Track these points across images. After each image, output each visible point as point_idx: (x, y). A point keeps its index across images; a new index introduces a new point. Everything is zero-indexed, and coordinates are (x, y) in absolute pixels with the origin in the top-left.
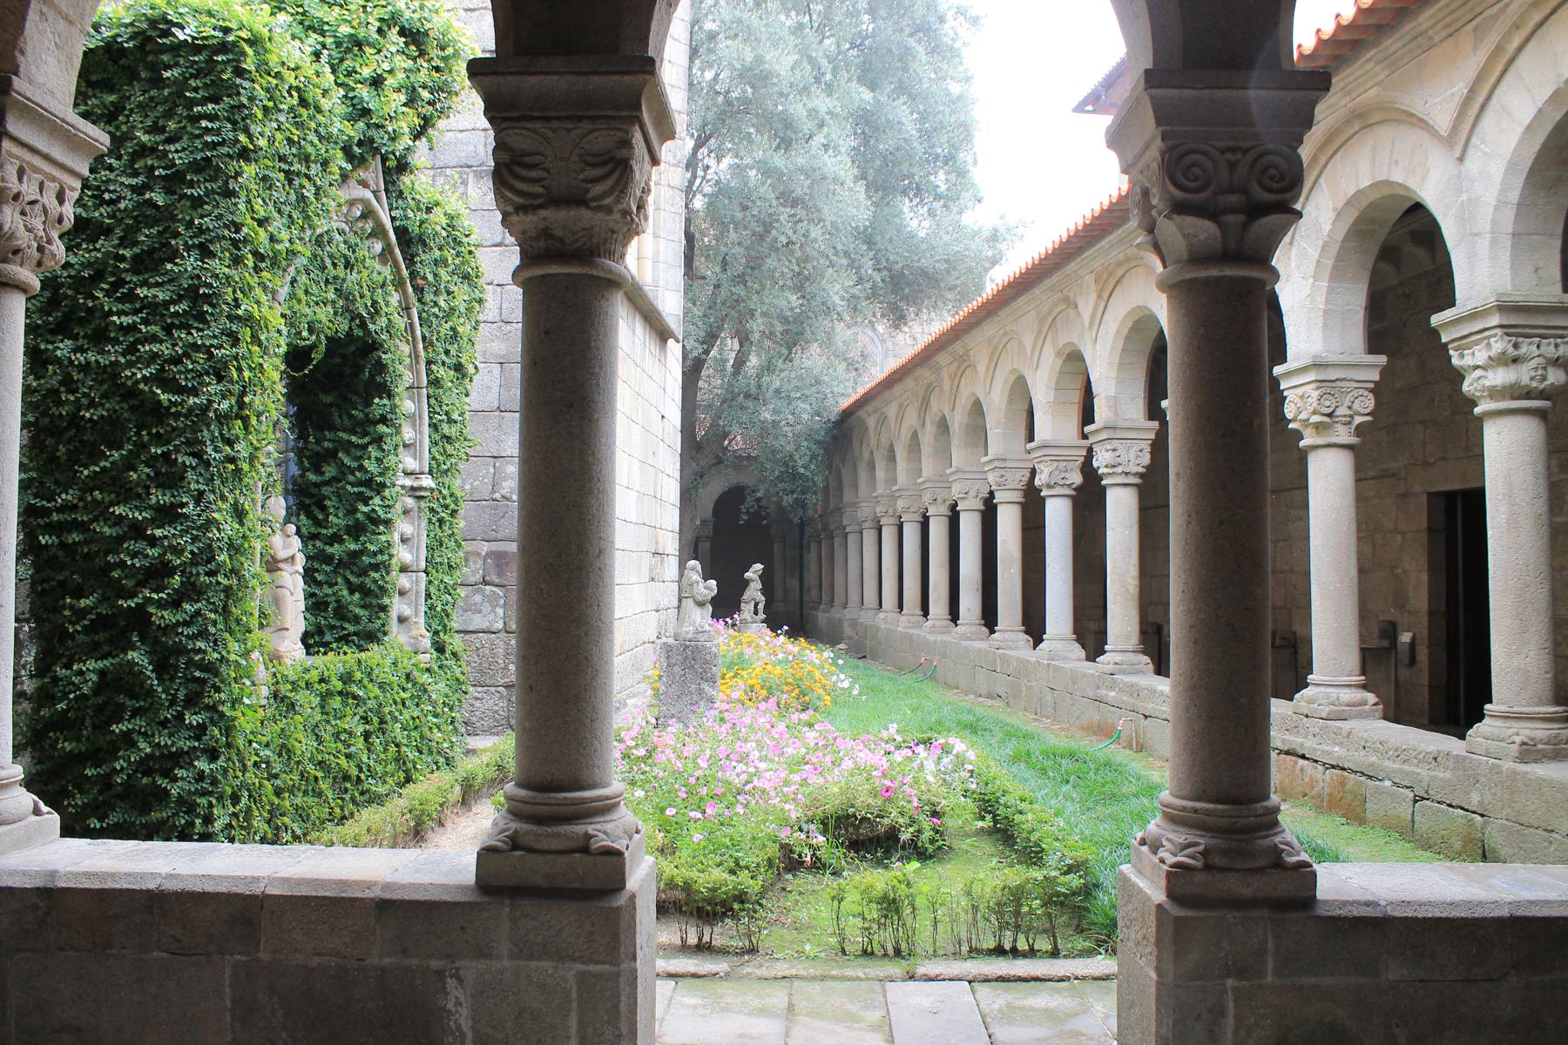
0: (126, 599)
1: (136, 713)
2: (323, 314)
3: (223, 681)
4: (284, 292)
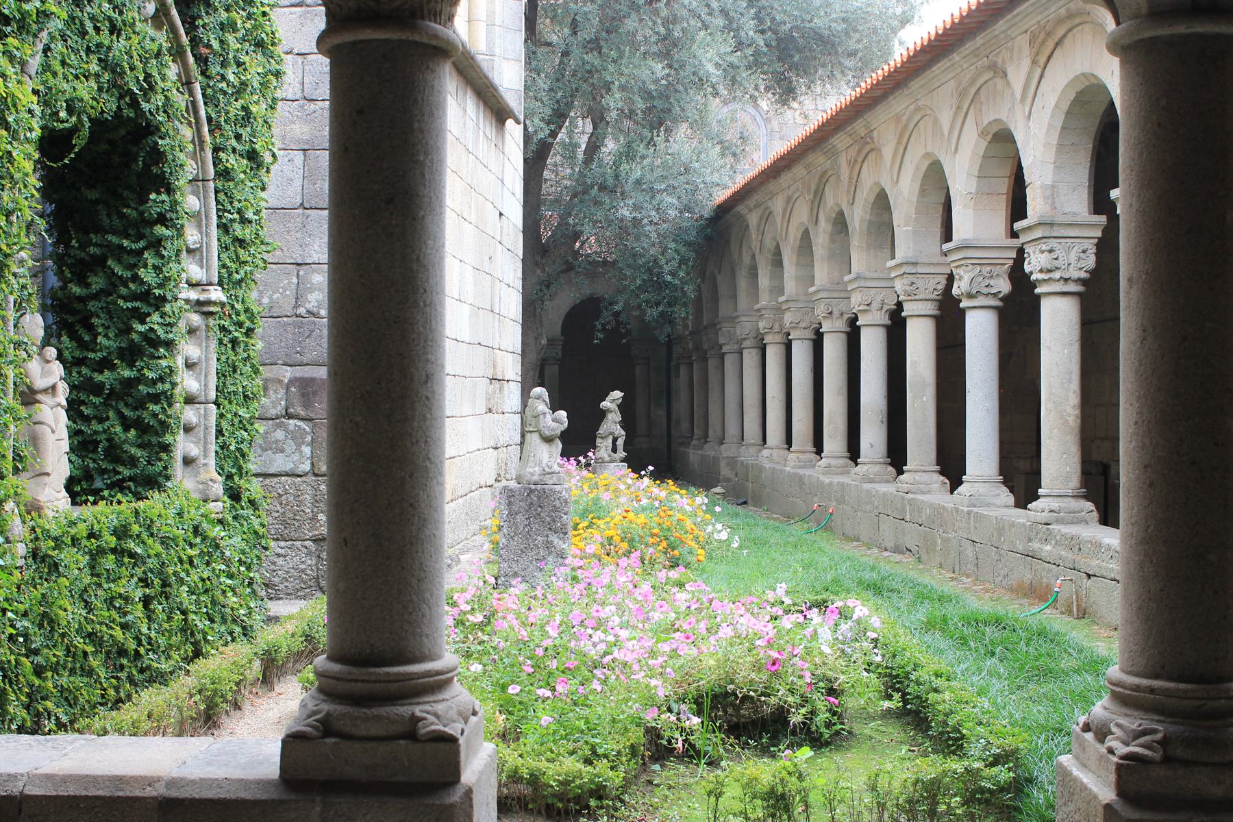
2: (85, 91)
4: (35, 63)
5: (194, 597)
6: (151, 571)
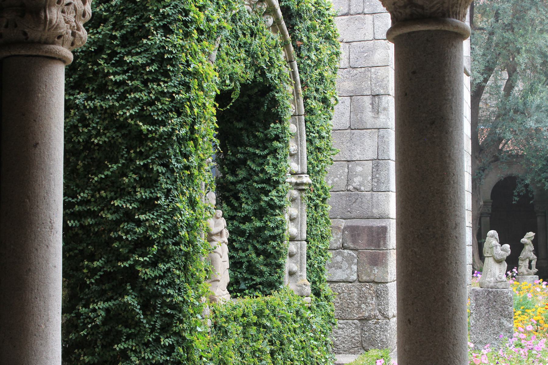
0: (122, 261)
1: (129, 337)
2: (239, 68)
3: (184, 316)
4: (214, 54)
5: (297, 351)
6: (274, 336)
